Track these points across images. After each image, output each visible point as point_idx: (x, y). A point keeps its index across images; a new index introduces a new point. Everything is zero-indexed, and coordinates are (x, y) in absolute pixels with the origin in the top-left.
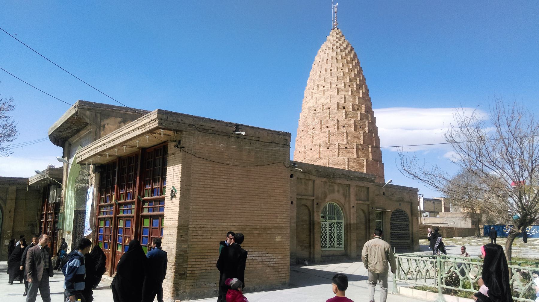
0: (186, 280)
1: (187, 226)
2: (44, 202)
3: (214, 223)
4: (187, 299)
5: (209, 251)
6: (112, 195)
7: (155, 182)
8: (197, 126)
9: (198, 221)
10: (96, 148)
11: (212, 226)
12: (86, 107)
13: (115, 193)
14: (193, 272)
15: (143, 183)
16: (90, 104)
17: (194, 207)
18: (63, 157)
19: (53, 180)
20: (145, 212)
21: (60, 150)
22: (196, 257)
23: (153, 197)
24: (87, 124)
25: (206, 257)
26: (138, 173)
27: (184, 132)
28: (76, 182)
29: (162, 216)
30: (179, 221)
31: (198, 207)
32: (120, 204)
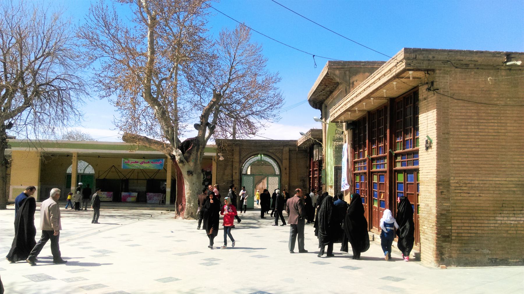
0: (451, 243)
1: (448, 181)
2: (310, 160)
3: (483, 178)
4: (454, 265)
5: (478, 211)
6: (364, 151)
7: (407, 134)
8: (453, 62)
9: (461, 175)
10: (345, 104)
11: (481, 182)
12: (335, 67)
13: (367, 149)
14: (460, 235)
15: (394, 136)
16: (339, 63)
17: (455, 159)
18: (321, 118)
19: (315, 141)
20: (399, 167)
21: (318, 112)
22: (462, 218)
23: (406, 150)
24: (338, 84)
25: (475, 218)
26: (388, 125)
27: (437, 71)
28: (334, 141)
29: (417, 171)
30: (438, 175)
31: (460, 158)
32: (373, 160)
